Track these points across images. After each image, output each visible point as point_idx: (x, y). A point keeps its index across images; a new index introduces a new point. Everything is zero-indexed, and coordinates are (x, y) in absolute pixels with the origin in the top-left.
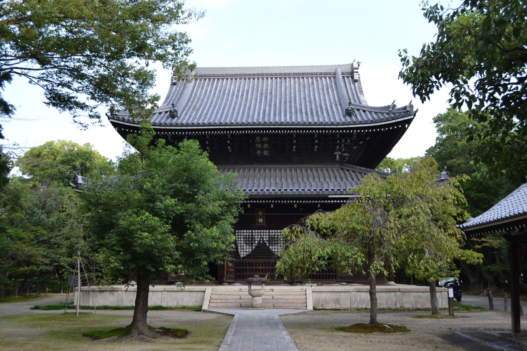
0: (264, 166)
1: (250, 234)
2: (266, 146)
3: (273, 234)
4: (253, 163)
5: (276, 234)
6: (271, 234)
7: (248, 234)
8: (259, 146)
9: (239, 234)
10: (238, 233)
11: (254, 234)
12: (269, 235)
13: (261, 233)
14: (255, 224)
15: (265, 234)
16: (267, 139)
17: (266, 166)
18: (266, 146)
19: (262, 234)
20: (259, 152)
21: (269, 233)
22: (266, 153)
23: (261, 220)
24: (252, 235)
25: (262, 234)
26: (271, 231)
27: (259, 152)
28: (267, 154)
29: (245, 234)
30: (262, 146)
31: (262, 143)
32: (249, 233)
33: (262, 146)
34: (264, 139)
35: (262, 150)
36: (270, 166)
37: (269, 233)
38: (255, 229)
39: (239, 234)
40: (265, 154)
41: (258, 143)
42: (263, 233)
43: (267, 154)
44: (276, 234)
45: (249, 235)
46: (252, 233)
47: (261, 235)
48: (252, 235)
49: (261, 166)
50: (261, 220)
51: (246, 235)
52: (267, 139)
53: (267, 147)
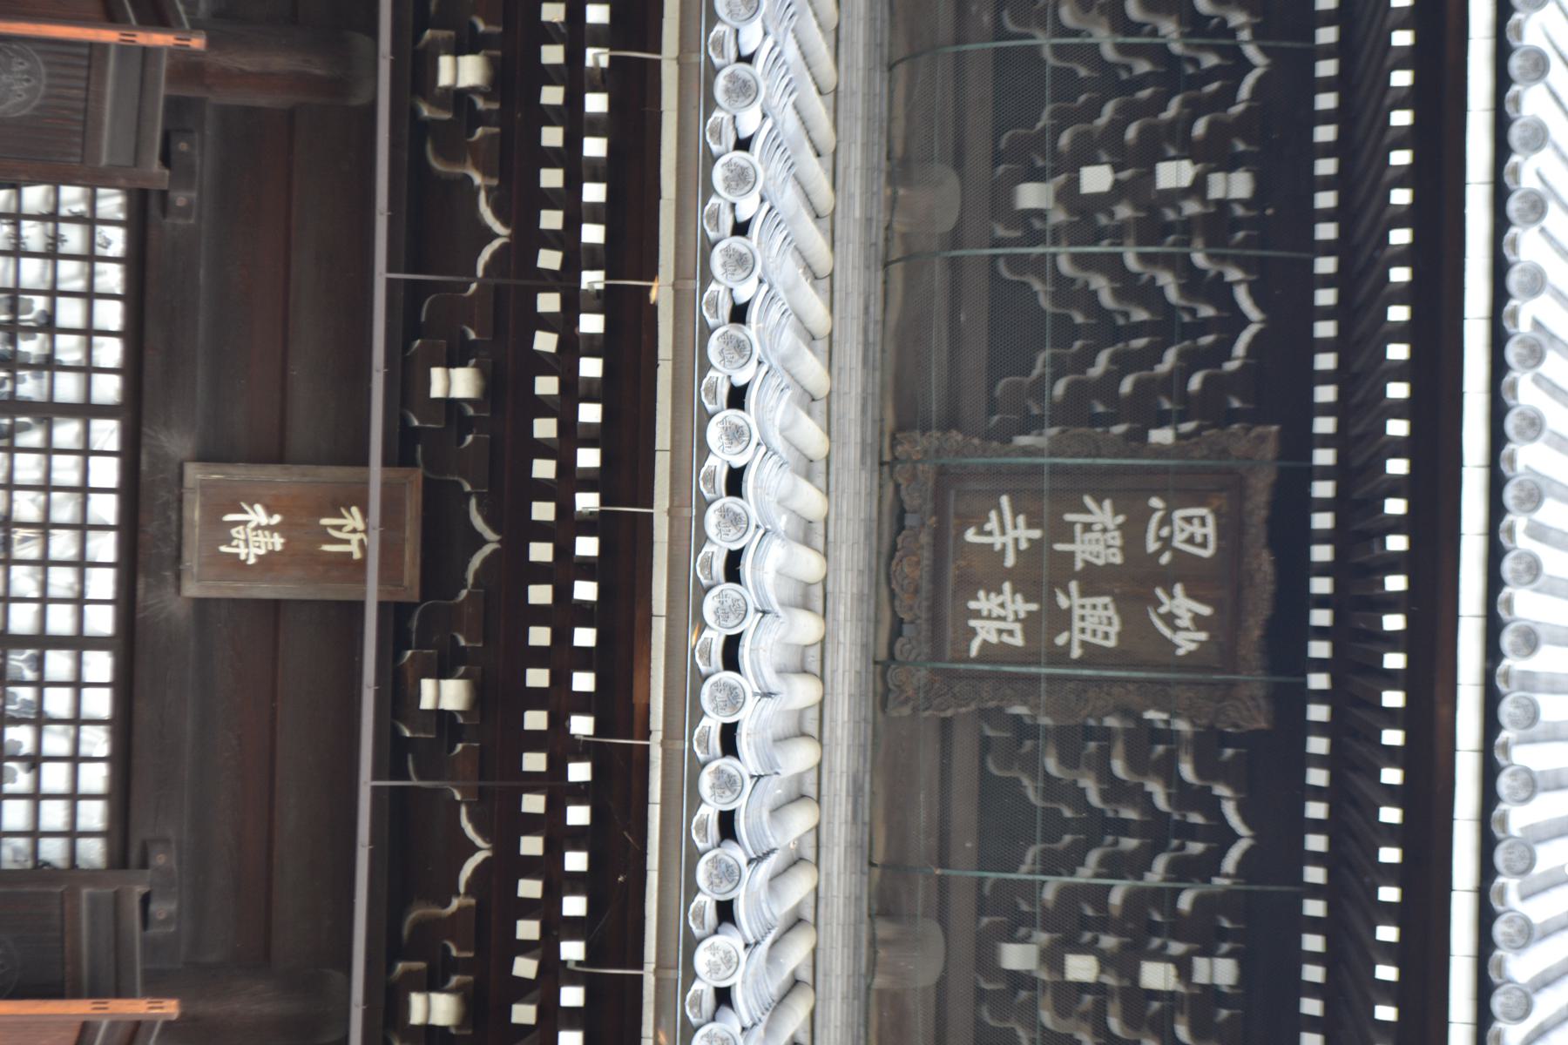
0: (847, 587)
1: (67, 388)
2: (1095, 621)
3: (58, 702)
4: (887, 462)
5: (56, 741)
6: (59, 663)
7: (69, 349)
8: (1097, 535)
9: (73, 237)
10: (89, 221)
11: (66, 432)
12: (42, 641)
13: (83, 527)
14: (206, 456)
15: (61, 581)
16: (1187, 642)
17: (844, 609)
18: (1095, 621)
19: (63, 545)
20: (1006, 532)
21: (79, 643)
22: (997, 617)
23: (255, 534)
24: (48, 411)
25: (63, 545)
26: (100, 665)
27: (1006, 532)
28: (986, 632)
29: (70, 313)
30: (1094, 580)
31: (1134, 582)
32: (87, 369)
33: (1094, 580)
34: (1182, 605)
35: (1042, 574)
36: (846, 662)
37: (79, 643)
38: (130, 454)
39: (73, 237)
40: (983, 602)
41: (1133, 534)
42: (90, 257)
43: (986, 632)
44: (56, 741)
45: (49, 364)
46: (86, 411)
47: (45, 527)
48: (48, 411)
49: (853, 555)
50: (255, 534)
51: (49, 325)
52: (1187, 642)
53: (1073, 641)
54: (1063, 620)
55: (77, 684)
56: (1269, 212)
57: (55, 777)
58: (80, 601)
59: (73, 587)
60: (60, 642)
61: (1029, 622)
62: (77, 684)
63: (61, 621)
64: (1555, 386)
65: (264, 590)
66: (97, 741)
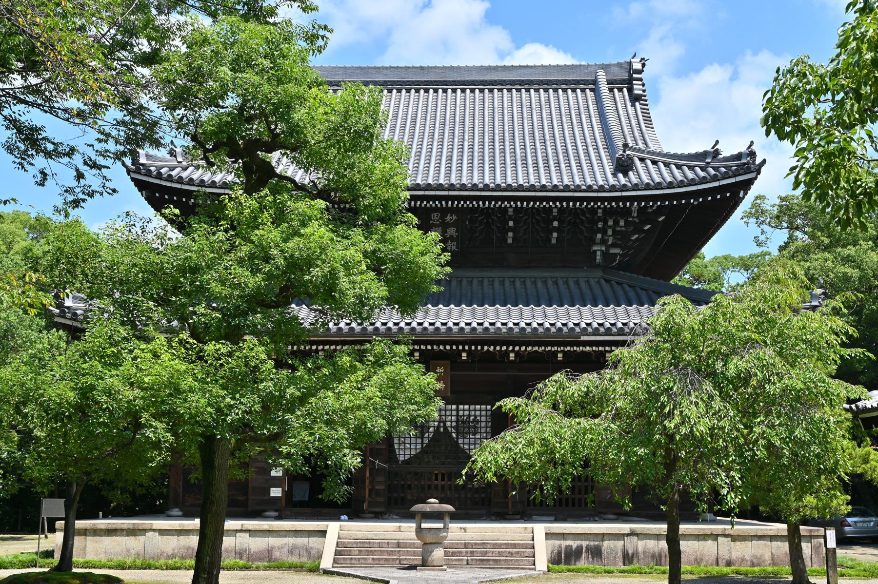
3: (466, 413)
6: (461, 413)
12: (457, 415)
16: (455, 217)
21: (457, 410)
34: (448, 218)
52: (455, 217)
53: (455, 235)
54: (451, 236)
55: (464, 410)
56: (701, 200)
57: (478, 413)
58: (451, 410)
59: (449, 574)
60: (458, 413)
61: (452, 242)
62: (464, 410)
63: (454, 413)
64: (771, 536)
65: (449, 384)
66: (472, 407)
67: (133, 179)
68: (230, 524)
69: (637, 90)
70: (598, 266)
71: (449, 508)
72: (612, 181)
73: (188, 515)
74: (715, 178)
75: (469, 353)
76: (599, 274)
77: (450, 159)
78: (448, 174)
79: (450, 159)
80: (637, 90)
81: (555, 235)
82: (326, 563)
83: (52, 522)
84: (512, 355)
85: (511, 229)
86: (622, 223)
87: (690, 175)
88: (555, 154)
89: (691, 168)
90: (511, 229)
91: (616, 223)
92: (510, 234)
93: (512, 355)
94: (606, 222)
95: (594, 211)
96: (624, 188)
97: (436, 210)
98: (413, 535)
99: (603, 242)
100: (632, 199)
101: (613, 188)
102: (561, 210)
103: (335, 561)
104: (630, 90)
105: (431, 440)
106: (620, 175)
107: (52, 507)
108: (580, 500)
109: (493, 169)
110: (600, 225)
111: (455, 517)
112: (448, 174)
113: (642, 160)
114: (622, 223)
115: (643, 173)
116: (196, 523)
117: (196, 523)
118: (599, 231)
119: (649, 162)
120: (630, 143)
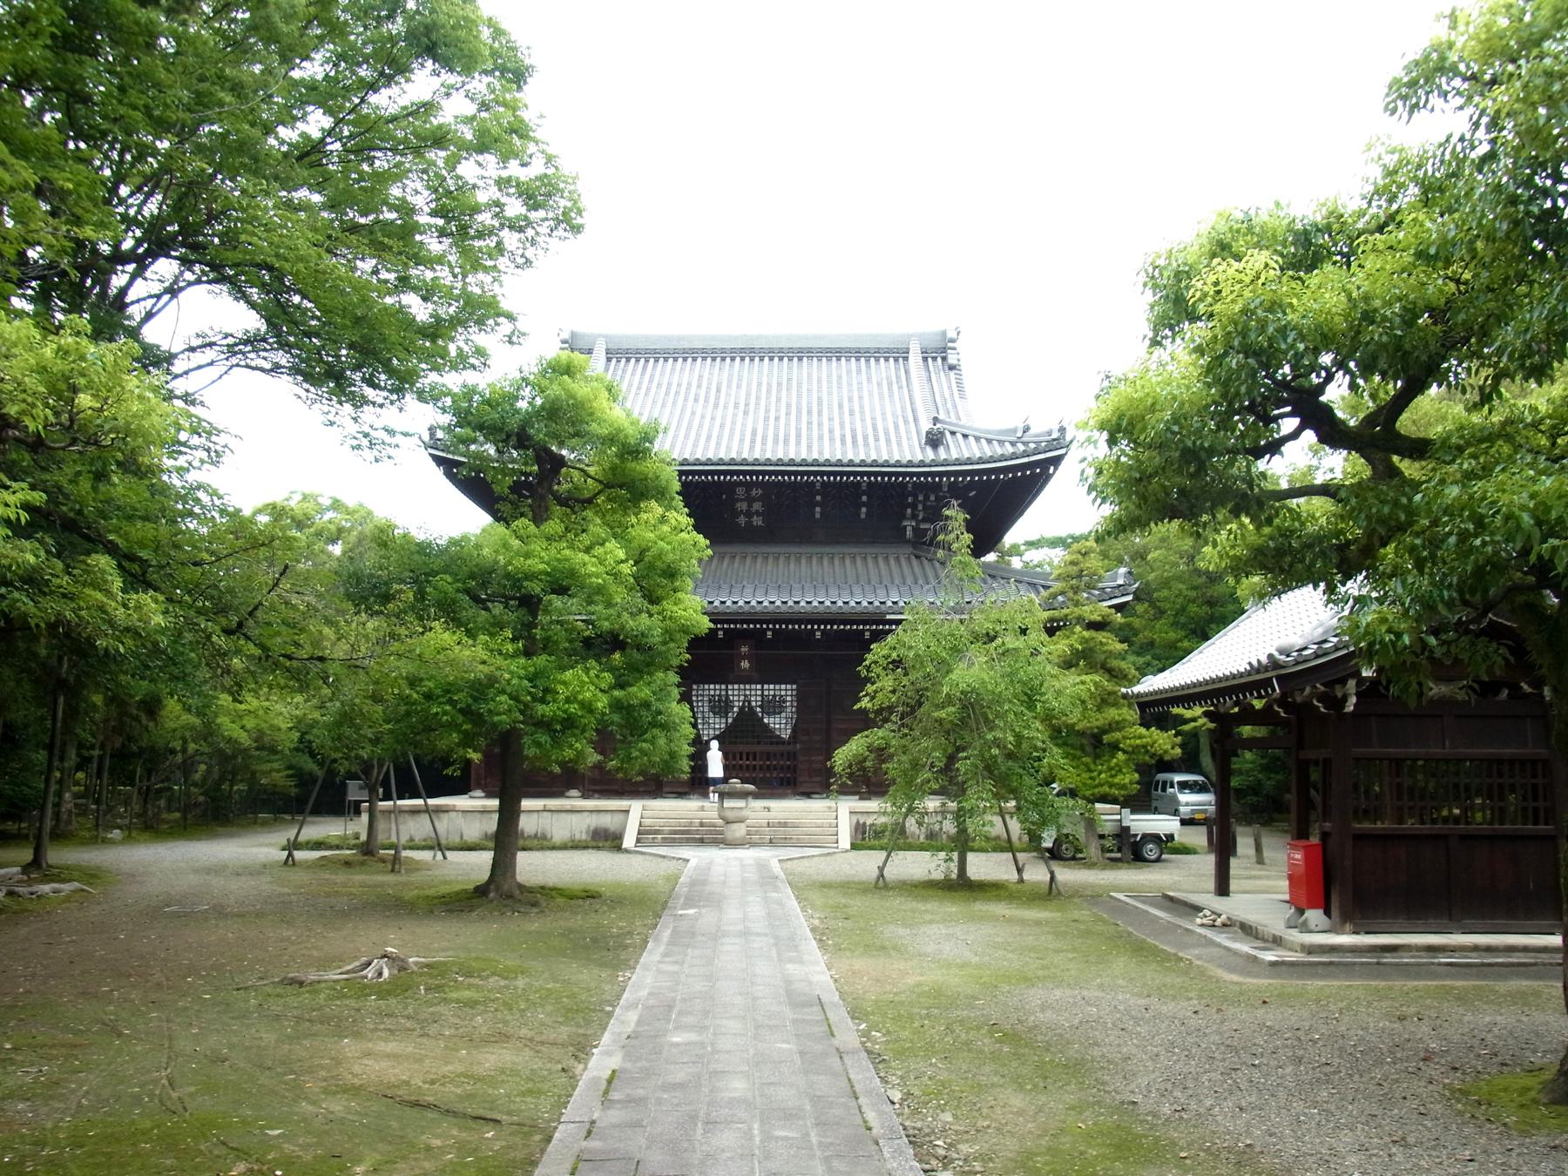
34: (754, 492)
67: (435, 458)
68: (526, 804)
69: (952, 360)
70: (909, 541)
71: (751, 787)
72: (920, 457)
73: (489, 795)
74: (1025, 454)
75: (774, 630)
76: (909, 550)
77: (687, 436)
78: (752, 448)
79: (687, 436)
80: (952, 360)
81: (864, 510)
82: (629, 841)
83: (357, 804)
84: (818, 634)
85: (864, 504)
86: (932, 498)
87: (999, 451)
88: (868, 427)
89: (1001, 442)
90: (864, 504)
91: (927, 498)
92: (864, 510)
93: (818, 634)
94: (916, 497)
95: (903, 485)
96: (934, 463)
97: (740, 484)
98: (715, 814)
99: (914, 517)
100: (941, 474)
101: (922, 464)
102: (951, 485)
103: (638, 841)
104: (944, 359)
105: (735, 720)
106: (929, 449)
107: (355, 791)
108: (1535, 799)
109: (798, 443)
110: (910, 500)
111: (756, 796)
112: (752, 448)
113: (953, 433)
114: (932, 498)
115: (957, 451)
116: (495, 803)
117: (495, 803)
118: (909, 505)
119: (959, 436)
120: (941, 417)
